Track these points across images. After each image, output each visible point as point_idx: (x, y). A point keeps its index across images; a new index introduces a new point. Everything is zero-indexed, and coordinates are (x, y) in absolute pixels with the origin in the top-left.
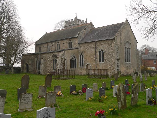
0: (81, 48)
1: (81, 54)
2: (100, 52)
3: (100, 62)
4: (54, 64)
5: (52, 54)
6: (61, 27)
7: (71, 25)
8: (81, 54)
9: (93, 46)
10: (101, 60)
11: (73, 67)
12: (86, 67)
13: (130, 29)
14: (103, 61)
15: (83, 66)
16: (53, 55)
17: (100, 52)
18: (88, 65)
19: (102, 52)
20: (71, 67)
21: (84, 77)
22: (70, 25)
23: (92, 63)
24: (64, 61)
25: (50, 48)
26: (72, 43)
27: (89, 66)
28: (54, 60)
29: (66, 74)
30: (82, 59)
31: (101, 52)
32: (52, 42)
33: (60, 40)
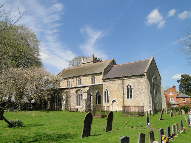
0: (106, 83)
1: (106, 89)
2: (128, 88)
3: (128, 98)
4: (77, 100)
5: (76, 90)
6: (152, 12)
7: (88, 63)
8: (106, 89)
9: (119, 82)
10: (130, 95)
11: (98, 103)
12: (111, 104)
13: (96, 86)
14: (131, 97)
15: (108, 102)
16: (77, 90)
17: (128, 88)
18: (114, 101)
19: (131, 87)
20: (96, 103)
21: (119, 113)
22: (87, 62)
23: (118, 99)
24: (90, 97)
25: (70, 83)
26: (96, 79)
27: (115, 102)
28: (78, 95)
29: (92, 110)
30: (107, 94)
31: (129, 88)
32: (72, 78)
33: (82, 76)
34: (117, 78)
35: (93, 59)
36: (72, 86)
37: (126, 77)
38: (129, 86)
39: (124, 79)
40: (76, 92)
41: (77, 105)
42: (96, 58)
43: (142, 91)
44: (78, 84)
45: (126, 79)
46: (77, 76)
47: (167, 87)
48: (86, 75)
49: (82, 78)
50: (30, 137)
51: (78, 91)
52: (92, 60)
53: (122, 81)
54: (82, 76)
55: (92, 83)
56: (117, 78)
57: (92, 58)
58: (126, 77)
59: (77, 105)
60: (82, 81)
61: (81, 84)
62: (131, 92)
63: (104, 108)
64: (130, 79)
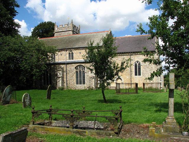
3: (136, 75)
14: (140, 75)
16: (78, 66)
19: (139, 64)
22: (63, 31)
31: (138, 64)
33: (74, 48)
34: (123, 53)
35: (72, 28)
36: (59, 61)
37: (134, 53)
38: (137, 62)
39: (132, 55)
40: (76, 68)
41: (77, 83)
42: (75, 26)
43: (152, 68)
44: (68, 58)
45: (134, 55)
46: (67, 49)
47: (137, 62)
48: (80, 48)
49: (75, 52)
50: (137, 110)
51: (78, 67)
52: (71, 28)
53: (130, 56)
54: (74, 48)
55: (70, 59)
56: (123, 53)
57: (71, 25)
58: (134, 53)
59: (77, 83)
60: (74, 54)
61: (73, 59)
62: (140, 69)
63: (121, 85)
64: (138, 55)
